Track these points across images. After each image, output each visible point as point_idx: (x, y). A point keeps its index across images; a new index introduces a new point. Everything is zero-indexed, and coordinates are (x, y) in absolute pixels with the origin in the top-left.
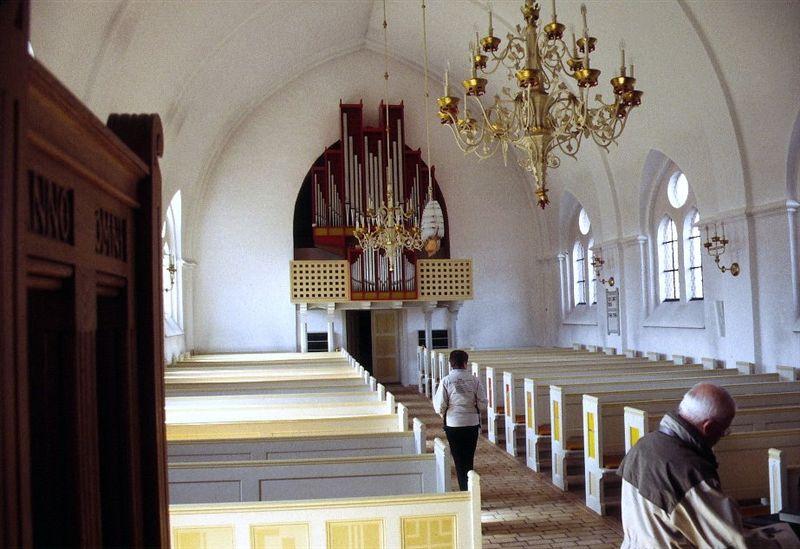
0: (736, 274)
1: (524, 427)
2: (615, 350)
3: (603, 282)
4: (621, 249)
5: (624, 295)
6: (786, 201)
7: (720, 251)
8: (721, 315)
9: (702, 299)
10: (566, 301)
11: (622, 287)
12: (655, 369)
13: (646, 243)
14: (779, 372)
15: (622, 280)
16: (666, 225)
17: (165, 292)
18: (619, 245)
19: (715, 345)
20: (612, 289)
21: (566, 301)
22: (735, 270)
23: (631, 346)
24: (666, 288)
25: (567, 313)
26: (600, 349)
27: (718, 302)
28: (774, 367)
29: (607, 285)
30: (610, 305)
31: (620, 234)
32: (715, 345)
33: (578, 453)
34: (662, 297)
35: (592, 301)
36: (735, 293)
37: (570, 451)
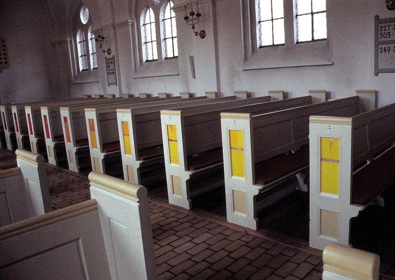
0: (203, 37)
1: (64, 143)
2: (114, 96)
3: (104, 52)
4: (115, 29)
5: (118, 61)
6: (127, 19)
7: (195, 21)
8: (193, 64)
9: (97, 68)
10: (74, 68)
11: (117, 54)
12: (145, 101)
13: (133, 25)
14: (271, 95)
15: (117, 49)
16: (145, 13)
17: (263, 207)
18: (114, 25)
19: (186, 83)
20: (111, 56)
21: (74, 68)
22: (203, 35)
23: (125, 91)
24: (150, 52)
25: (75, 76)
26: (101, 97)
27: (190, 57)
28: (179, 93)
29: (106, 54)
30: (108, 67)
31: (114, 20)
32: (186, 83)
33: (118, 152)
34: (144, 60)
35: (92, 67)
36: (202, 51)
37: (56, 142)
